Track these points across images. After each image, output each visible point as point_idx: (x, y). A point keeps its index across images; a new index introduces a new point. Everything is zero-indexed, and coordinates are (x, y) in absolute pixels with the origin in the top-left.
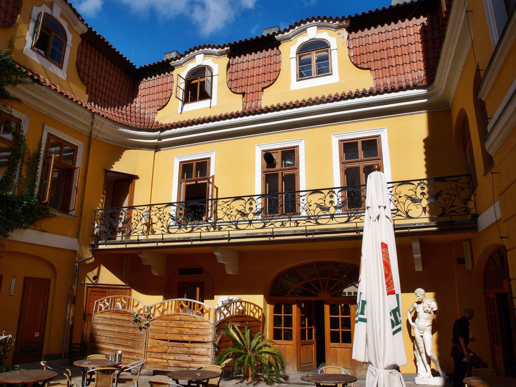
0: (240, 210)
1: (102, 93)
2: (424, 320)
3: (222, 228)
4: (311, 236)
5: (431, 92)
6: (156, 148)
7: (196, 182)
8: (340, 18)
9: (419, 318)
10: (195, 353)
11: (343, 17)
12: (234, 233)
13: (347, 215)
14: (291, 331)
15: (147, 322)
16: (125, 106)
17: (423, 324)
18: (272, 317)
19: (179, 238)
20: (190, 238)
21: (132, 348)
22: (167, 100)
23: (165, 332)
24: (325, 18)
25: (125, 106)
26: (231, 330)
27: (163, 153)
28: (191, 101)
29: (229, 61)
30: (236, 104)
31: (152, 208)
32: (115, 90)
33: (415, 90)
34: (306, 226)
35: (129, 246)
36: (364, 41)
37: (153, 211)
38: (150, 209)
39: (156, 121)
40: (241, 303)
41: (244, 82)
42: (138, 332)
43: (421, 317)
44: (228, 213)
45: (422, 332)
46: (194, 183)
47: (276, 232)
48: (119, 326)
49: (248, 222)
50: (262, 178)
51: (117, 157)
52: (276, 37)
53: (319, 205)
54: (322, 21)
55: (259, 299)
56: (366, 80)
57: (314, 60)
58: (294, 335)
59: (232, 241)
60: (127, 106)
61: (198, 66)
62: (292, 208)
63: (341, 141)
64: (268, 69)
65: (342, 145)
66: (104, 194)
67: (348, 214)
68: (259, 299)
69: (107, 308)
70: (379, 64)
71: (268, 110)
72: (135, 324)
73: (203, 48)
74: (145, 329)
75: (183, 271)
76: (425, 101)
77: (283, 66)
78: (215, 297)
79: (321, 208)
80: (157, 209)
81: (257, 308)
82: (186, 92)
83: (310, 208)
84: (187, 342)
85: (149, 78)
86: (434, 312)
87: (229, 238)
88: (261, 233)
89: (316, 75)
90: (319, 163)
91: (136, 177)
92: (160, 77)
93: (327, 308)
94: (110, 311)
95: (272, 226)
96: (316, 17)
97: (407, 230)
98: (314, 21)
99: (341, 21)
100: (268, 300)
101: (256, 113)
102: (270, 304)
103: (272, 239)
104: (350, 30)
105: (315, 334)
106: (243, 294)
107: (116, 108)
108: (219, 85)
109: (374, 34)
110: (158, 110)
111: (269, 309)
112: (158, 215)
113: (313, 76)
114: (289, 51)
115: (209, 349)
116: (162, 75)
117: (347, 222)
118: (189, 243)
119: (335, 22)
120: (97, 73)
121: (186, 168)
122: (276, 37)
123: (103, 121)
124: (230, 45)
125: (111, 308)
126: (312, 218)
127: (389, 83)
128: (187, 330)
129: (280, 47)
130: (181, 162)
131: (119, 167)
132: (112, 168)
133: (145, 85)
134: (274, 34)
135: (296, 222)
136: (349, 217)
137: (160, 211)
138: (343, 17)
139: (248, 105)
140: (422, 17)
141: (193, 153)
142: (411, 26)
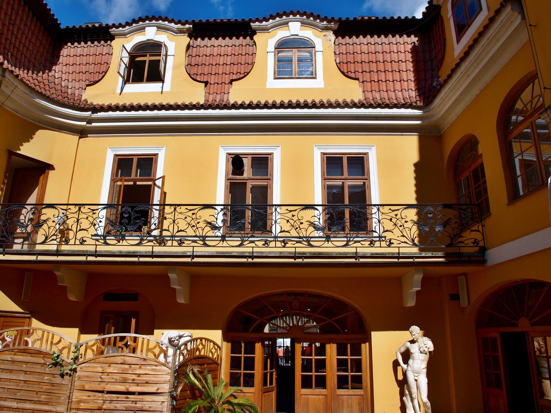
0: (209, 221)
1: (14, 47)
2: (420, 362)
4: (300, 260)
5: (427, 114)
6: (82, 133)
7: (135, 183)
8: (329, 18)
9: (414, 359)
10: (144, 408)
11: (333, 18)
12: (200, 250)
13: (346, 239)
14: (253, 375)
15: (74, 366)
16: (41, 73)
17: (419, 366)
18: (229, 358)
19: (121, 252)
20: (137, 252)
21: (46, 404)
22: (101, 76)
23: (100, 380)
24: (312, 15)
25: (41, 73)
26: (191, 376)
27: (91, 141)
28: (132, 82)
30: (197, 93)
31: (82, 209)
32: (31, 48)
33: (410, 109)
34: (295, 247)
35: (400, 260)
36: (351, 49)
37: (84, 213)
38: (79, 209)
39: (83, 98)
40: (201, 340)
41: (206, 70)
42: (58, 380)
43: (416, 358)
44: (194, 224)
45: (417, 375)
46: (132, 183)
47: (257, 252)
48: (26, 372)
50: (226, 186)
51: (28, 137)
52: (252, 24)
53: (312, 223)
54: (308, 17)
55: (216, 335)
56: (354, 91)
57: (293, 58)
59: (196, 260)
60: (43, 73)
61: (148, 40)
62: (261, 224)
63: (324, 154)
64: (243, 59)
65: (325, 159)
66: (4, 183)
68: (216, 335)
69: (7, 345)
70: (367, 76)
71: (234, 106)
72: (53, 369)
73: (157, 20)
74: (70, 375)
75: (109, 297)
77: (258, 59)
78: (156, 331)
79: (314, 227)
80: (89, 211)
81: (216, 347)
82: (129, 68)
83: (301, 226)
84: (133, 393)
85: (76, 44)
86: (430, 352)
87: (193, 257)
88: (236, 252)
89: (297, 76)
90: (297, 177)
91: (50, 167)
92: (92, 45)
94: (12, 350)
96: (302, 12)
97: (412, 260)
98: (298, 16)
99: (329, 22)
100: (226, 338)
101: (218, 107)
102: (227, 342)
103: (250, 260)
104: (337, 33)
105: (276, 379)
106: (194, 329)
107: (30, 71)
108: (175, 67)
109: (363, 44)
110: (88, 86)
111: (226, 347)
112: (91, 219)
113: (294, 76)
114: (267, 42)
115: (163, 402)
116: (96, 43)
117: (346, 246)
118: (135, 259)
119: (323, 22)
120: (10, 19)
121: (123, 164)
122: (252, 24)
123: (16, 83)
124: (193, 23)
125: (14, 345)
126: (304, 239)
128: (134, 377)
129: (255, 38)
130: (116, 155)
131: (28, 150)
132: (20, 150)
133: (69, 52)
134: (251, 20)
137: (94, 213)
138: (333, 18)
139: (211, 98)
140: (413, 36)
141: (135, 146)
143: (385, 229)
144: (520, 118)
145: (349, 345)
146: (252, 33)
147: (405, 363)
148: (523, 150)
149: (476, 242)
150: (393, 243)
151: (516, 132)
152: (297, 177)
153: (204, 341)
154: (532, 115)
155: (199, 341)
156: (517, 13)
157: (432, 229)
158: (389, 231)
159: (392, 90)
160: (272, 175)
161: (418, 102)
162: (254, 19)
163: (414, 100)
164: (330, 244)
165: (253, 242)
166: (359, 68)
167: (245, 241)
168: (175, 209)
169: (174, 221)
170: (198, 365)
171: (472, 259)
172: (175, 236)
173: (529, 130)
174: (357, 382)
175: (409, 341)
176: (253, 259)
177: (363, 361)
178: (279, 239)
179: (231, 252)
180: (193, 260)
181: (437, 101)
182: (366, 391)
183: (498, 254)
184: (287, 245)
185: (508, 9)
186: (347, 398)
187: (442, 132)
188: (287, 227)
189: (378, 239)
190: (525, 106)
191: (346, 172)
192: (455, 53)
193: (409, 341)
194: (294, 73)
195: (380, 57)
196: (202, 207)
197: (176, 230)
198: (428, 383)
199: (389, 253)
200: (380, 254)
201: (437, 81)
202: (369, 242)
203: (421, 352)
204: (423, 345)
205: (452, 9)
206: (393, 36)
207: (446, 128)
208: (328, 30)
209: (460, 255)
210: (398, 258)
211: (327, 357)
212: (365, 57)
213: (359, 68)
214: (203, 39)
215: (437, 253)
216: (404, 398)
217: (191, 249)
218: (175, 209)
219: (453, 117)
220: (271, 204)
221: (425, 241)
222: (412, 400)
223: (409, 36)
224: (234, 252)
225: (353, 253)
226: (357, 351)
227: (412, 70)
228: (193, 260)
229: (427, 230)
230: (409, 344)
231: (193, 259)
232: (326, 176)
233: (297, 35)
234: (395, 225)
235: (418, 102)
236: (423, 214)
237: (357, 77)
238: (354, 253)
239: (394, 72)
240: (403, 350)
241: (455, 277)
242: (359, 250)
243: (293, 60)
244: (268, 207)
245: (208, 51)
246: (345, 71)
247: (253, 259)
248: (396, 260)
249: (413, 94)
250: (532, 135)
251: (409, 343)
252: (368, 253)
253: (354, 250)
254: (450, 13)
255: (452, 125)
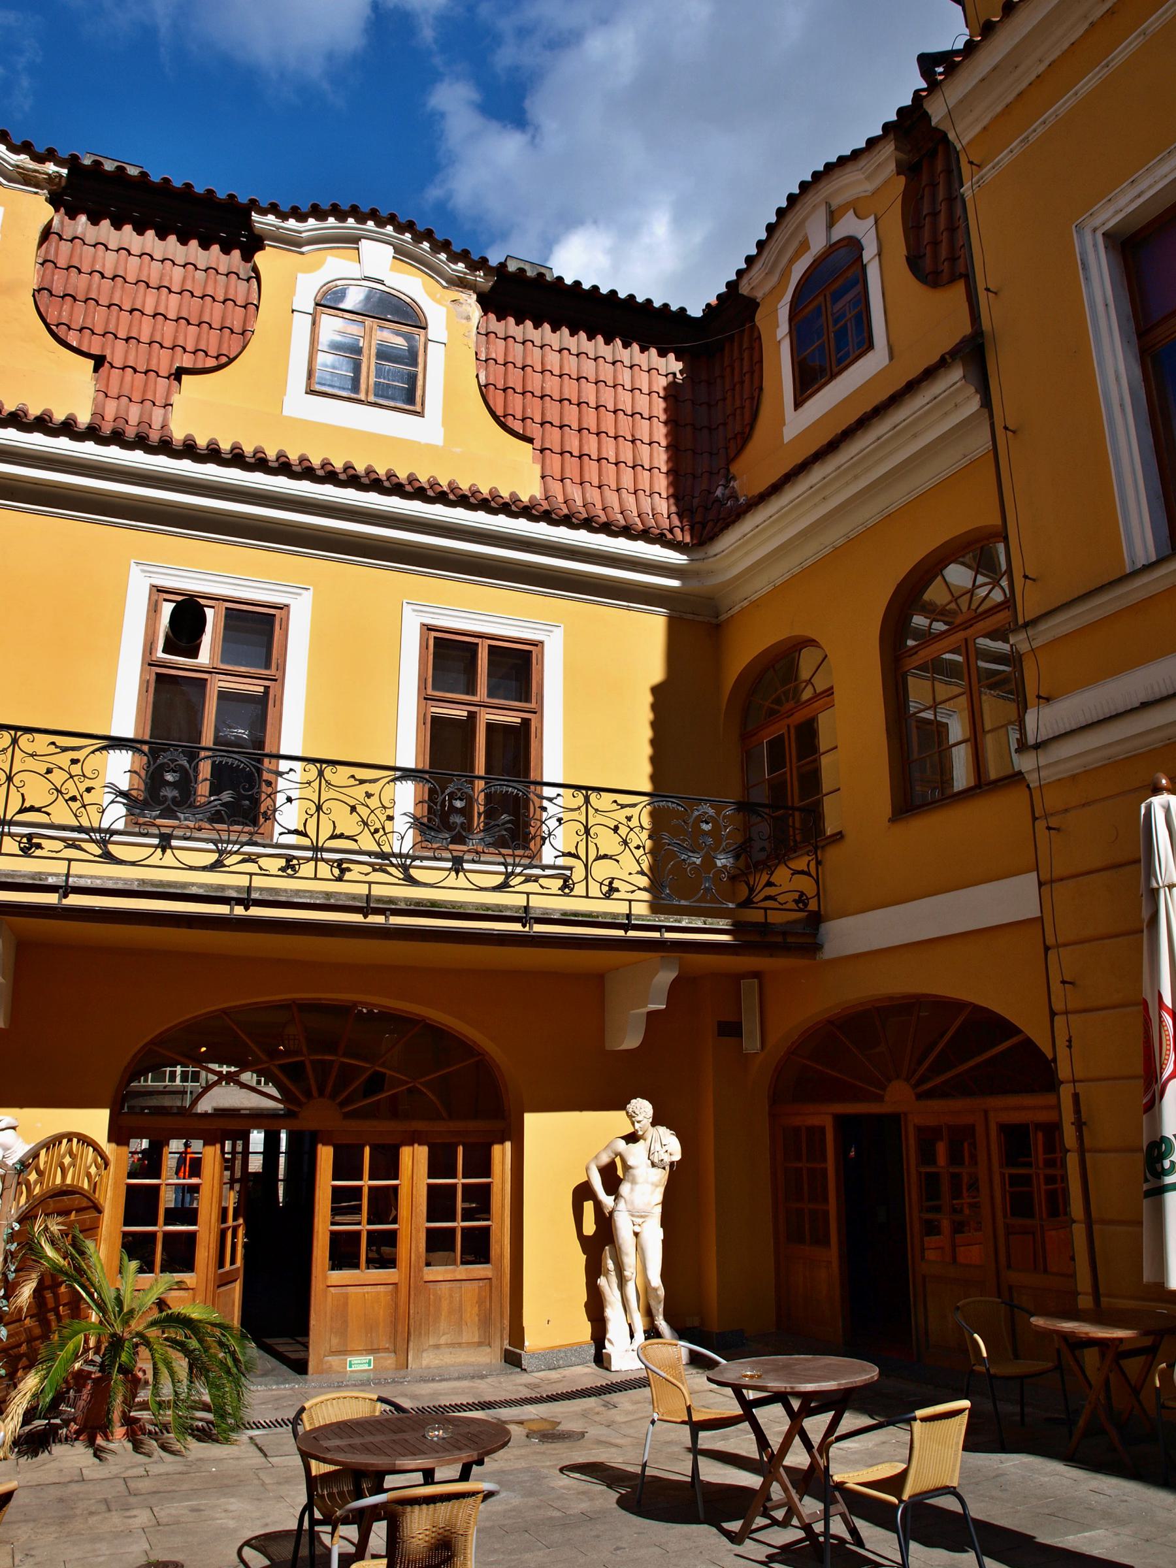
2: (649, 1188)
3: (39, 846)
4: (379, 919)
13: (502, 869)
24: (428, 235)
29: (52, 220)
33: (658, 546)
34: (370, 883)
35: (631, 933)
40: (70, 1140)
43: (640, 1179)
44: (73, 792)
45: (639, 1221)
47: (261, 889)
49: (449, 865)
52: (255, 216)
55: (94, 1122)
56: (517, 471)
58: (204, 1253)
59: (74, 900)
67: (505, 865)
71: (189, 450)
76: (675, 583)
87: (67, 890)
88: (201, 886)
89: (372, 399)
90: (349, 684)
93: (325, 1155)
95: (250, 867)
97: (656, 935)
101: (141, 443)
103: (239, 910)
104: (487, 302)
109: (552, 347)
113: (362, 396)
117: (502, 887)
119: (456, 263)
122: (255, 216)
124: (73, 162)
126: (394, 860)
127: (133, 419)
129: (259, 258)
134: (253, 205)
135: (339, 866)
136: (508, 875)
138: (484, 260)
140: (672, 356)
142: (223, 269)
143: (601, 853)
144: (939, 626)
145: (460, 1149)
146: (252, 244)
147: (608, 1193)
148: (938, 699)
149: (802, 899)
150: (617, 890)
151: (925, 655)
152: (349, 684)
153: (75, 1140)
154: (967, 624)
155: (65, 1141)
156: (972, 389)
157: (709, 861)
158: (611, 858)
159: (614, 487)
160: (282, 667)
161: (678, 531)
162: (264, 204)
163: (665, 524)
164: (462, 881)
165: (250, 859)
166: (535, 409)
167: (231, 853)
168: (15, 741)
169: (319, 808)
170: (60, 1214)
171: (790, 940)
172: (323, 850)
173: (959, 658)
174: (477, 1248)
175: (623, 1138)
176: (247, 909)
177: (403, 1194)
178: (326, 855)
179: (185, 885)
180: (65, 902)
181: (729, 540)
182: (499, 1269)
183: (849, 935)
184: (347, 876)
185: (956, 374)
186: (451, 1289)
187: (724, 617)
188: (348, 824)
189: (309, 854)
190: (955, 599)
191: (482, 683)
192: (785, 430)
193: (623, 1138)
194: (363, 386)
195: (589, 393)
196: (104, 743)
197: (325, 832)
198: (664, 1241)
199: (605, 914)
200: (583, 915)
201: (726, 487)
202: (560, 882)
203: (653, 1165)
204: (658, 1147)
205: (791, 320)
206: (626, 345)
207: (737, 608)
208: (465, 287)
209: (764, 928)
210: (625, 927)
211: (403, 1182)
212: (552, 385)
213: (535, 409)
214: (95, 220)
215: (662, 917)
216: (602, 1281)
217: (61, 868)
218: (15, 741)
219: (761, 585)
220: (274, 752)
221: (665, 882)
222: (622, 1282)
223: (662, 354)
224: (193, 884)
225: (518, 908)
226: (481, 1165)
227: (664, 443)
228: (65, 902)
229: (698, 861)
230: (621, 1145)
231: (66, 896)
232: (430, 691)
233: (381, 282)
234: (625, 843)
235: (678, 531)
236: (691, 820)
237: (529, 434)
238: (519, 908)
239: (621, 439)
240: (605, 1159)
241: (737, 978)
242: (535, 901)
243: (365, 351)
244: (266, 760)
245: (109, 262)
246: (500, 412)
247: (247, 909)
248: (621, 933)
249: (663, 506)
250: (965, 671)
251: (623, 1142)
252: (554, 910)
253: (521, 901)
254: (783, 329)
255: (755, 604)
